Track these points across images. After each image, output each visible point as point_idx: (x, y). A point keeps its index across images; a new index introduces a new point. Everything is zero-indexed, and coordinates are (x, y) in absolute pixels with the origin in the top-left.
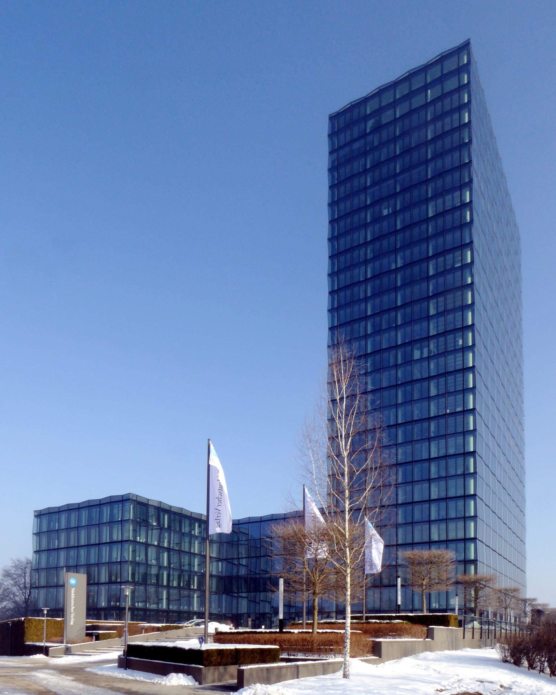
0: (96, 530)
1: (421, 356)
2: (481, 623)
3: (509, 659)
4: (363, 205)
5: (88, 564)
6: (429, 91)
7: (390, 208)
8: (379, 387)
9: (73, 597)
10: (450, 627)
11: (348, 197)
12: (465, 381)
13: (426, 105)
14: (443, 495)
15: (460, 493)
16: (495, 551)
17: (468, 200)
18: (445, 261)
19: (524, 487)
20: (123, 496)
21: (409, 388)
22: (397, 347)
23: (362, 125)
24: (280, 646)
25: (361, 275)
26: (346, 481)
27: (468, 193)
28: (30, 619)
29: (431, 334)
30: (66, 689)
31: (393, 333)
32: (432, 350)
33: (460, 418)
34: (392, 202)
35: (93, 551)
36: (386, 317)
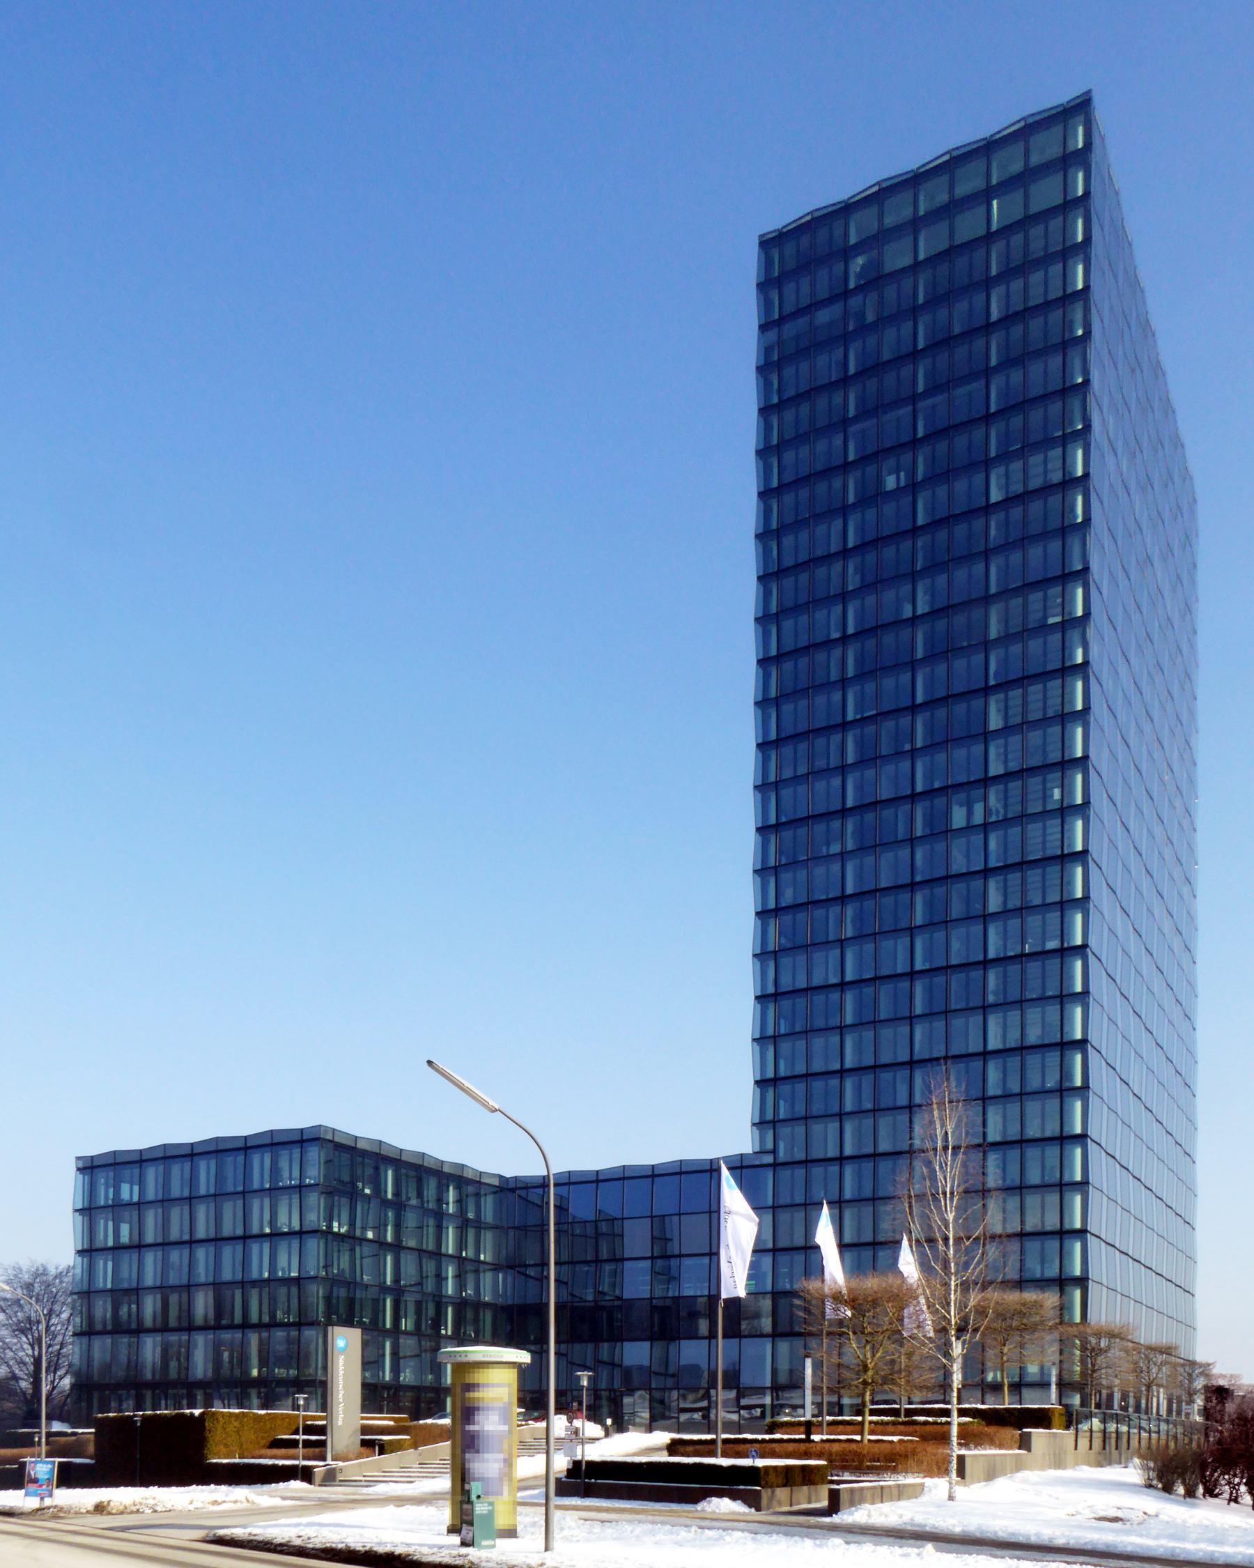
0: (235, 1207)
1: (968, 820)
2: (1104, 1421)
3: (1155, 1482)
4: (840, 461)
5: (217, 1281)
6: (995, 203)
7: (902, 474)
8: (873, 888)
9: (341, 1373)
10: (1054, 1431)
11: (801, 438)
12: (1065, 883)
13: (989, 237)
14: (1014, 1133)
15: (1052, 1129)
16: (1127, 1254)
17: (1080, 473)
18: (1025, 605)
19: (1194, 1096)
20: (302, 1130)
21: (940, 891)
22: (913, 797)
23: (839, 268)
24: (830, 1461)
25: (833, 627)
26: (952, 1252)
27: (1080, 453)
28: (214, 1414)
29: (992, 773)
30: (737, 1507)
31: (905, 765)
32: (994, 809)
33: (1053, 964)
34: (907, 457)
35: (229, 1253)
36: (889, 725)
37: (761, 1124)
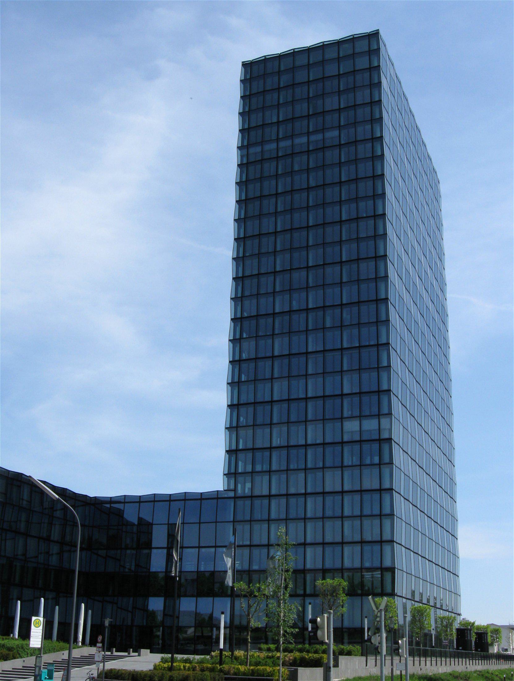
37: (228, 475)
